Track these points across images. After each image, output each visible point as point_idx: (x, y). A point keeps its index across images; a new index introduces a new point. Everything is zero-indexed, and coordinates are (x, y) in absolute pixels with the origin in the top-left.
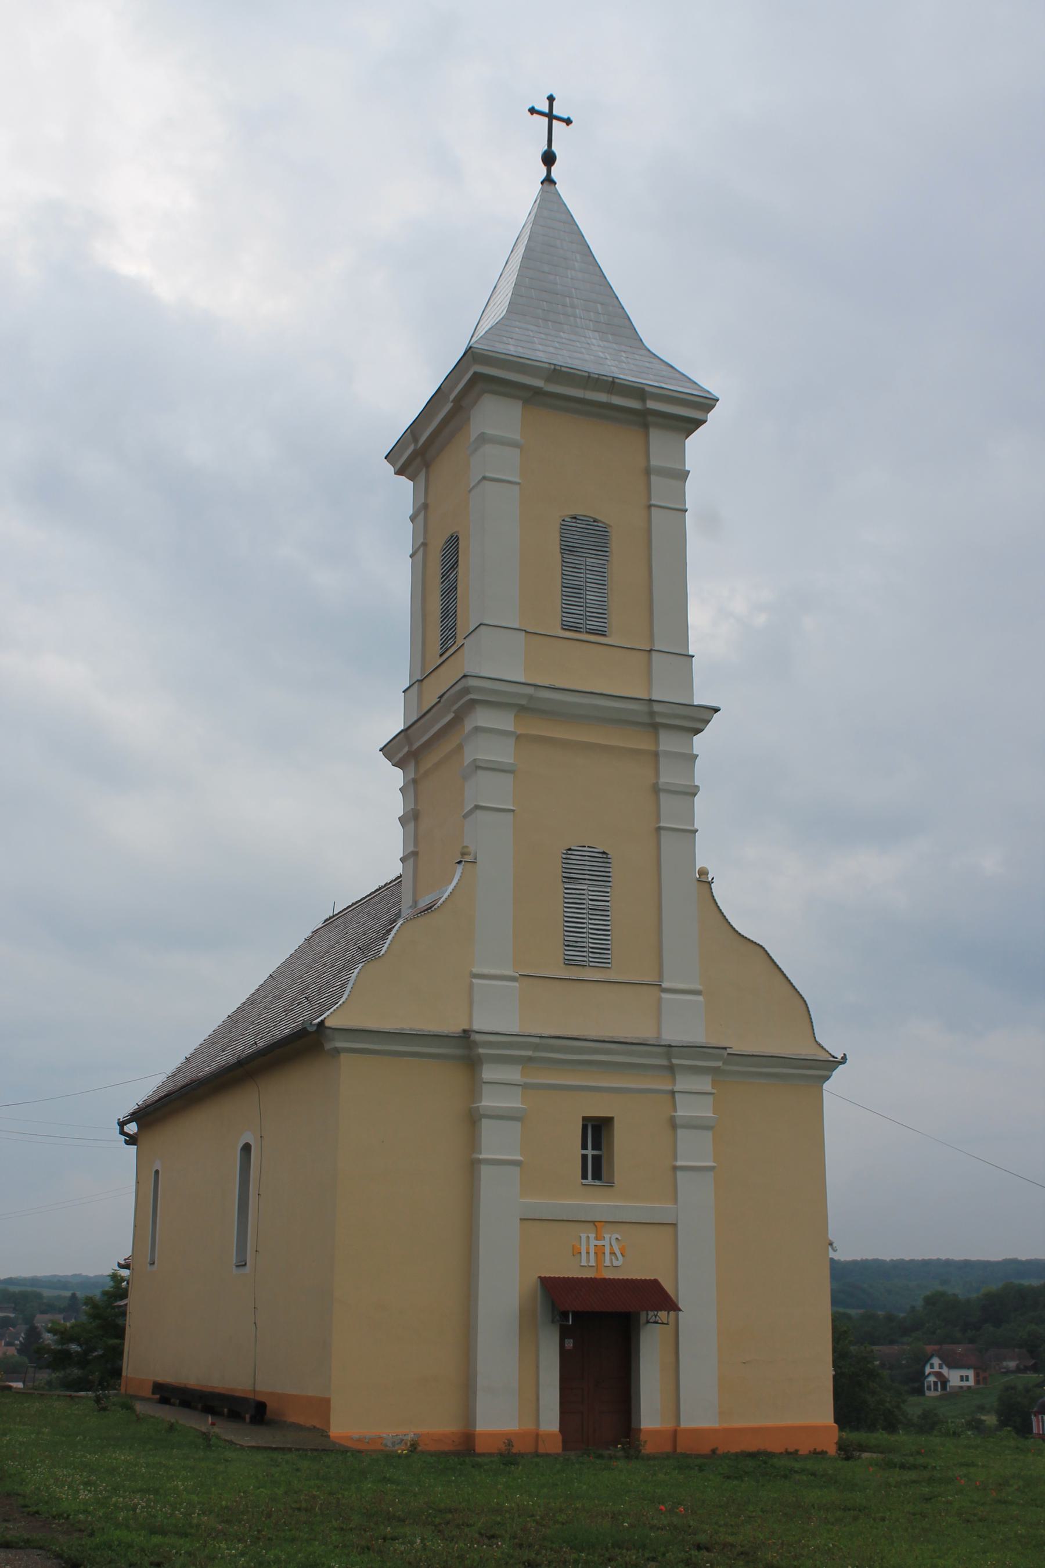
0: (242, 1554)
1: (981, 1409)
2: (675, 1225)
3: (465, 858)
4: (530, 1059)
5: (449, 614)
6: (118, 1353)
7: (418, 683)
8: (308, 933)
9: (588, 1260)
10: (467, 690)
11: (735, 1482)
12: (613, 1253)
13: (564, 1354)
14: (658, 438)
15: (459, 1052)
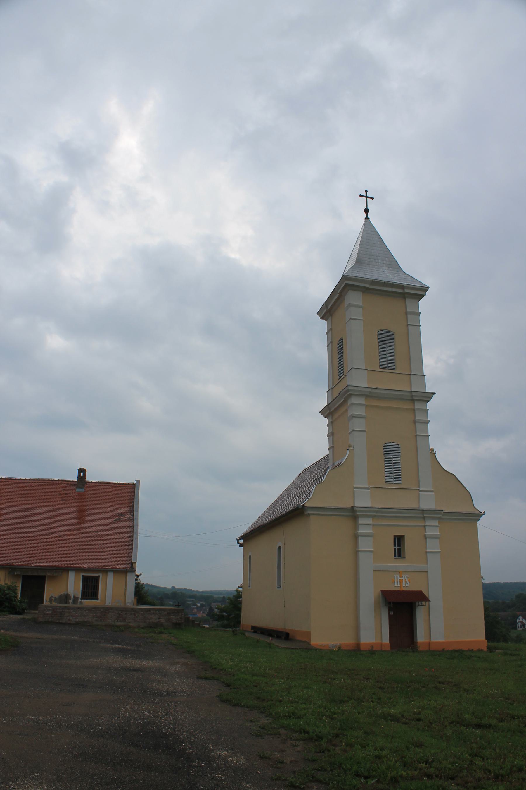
0: (284, 683)
2: (427, 572)
3: (350, 448)
4: (375, 516)
5: (341, 365)
6: (239, 616)
7: (331, 389)
10: (348, 391)
12: (406, 582)
13: (390, 617)
14: (409, 302)
15: (350, 514)
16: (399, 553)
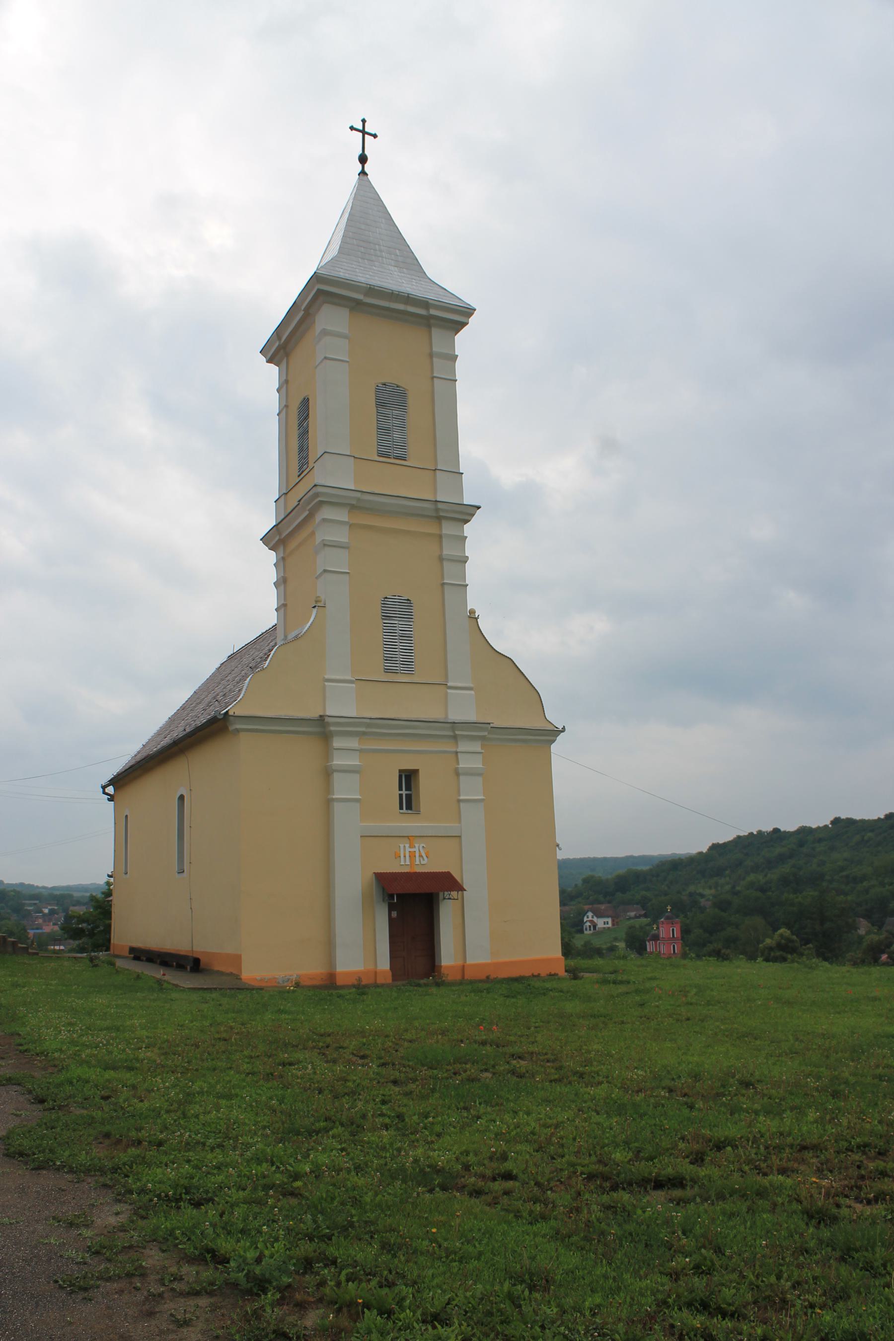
0: (174, 1086)
1: (616, 939)
2: (460, 837)
3: (318, 604)
4: (364, 733)
5: (303, 450)
6: (108, 928)
7: (284, 495)
8: (218, 665)
9: (405, 861)
10: (317, 495)
11: (513, 1000)
12: (421, 856)
13: (391, 920)
14: (437, 334)
16: (408, 803)
